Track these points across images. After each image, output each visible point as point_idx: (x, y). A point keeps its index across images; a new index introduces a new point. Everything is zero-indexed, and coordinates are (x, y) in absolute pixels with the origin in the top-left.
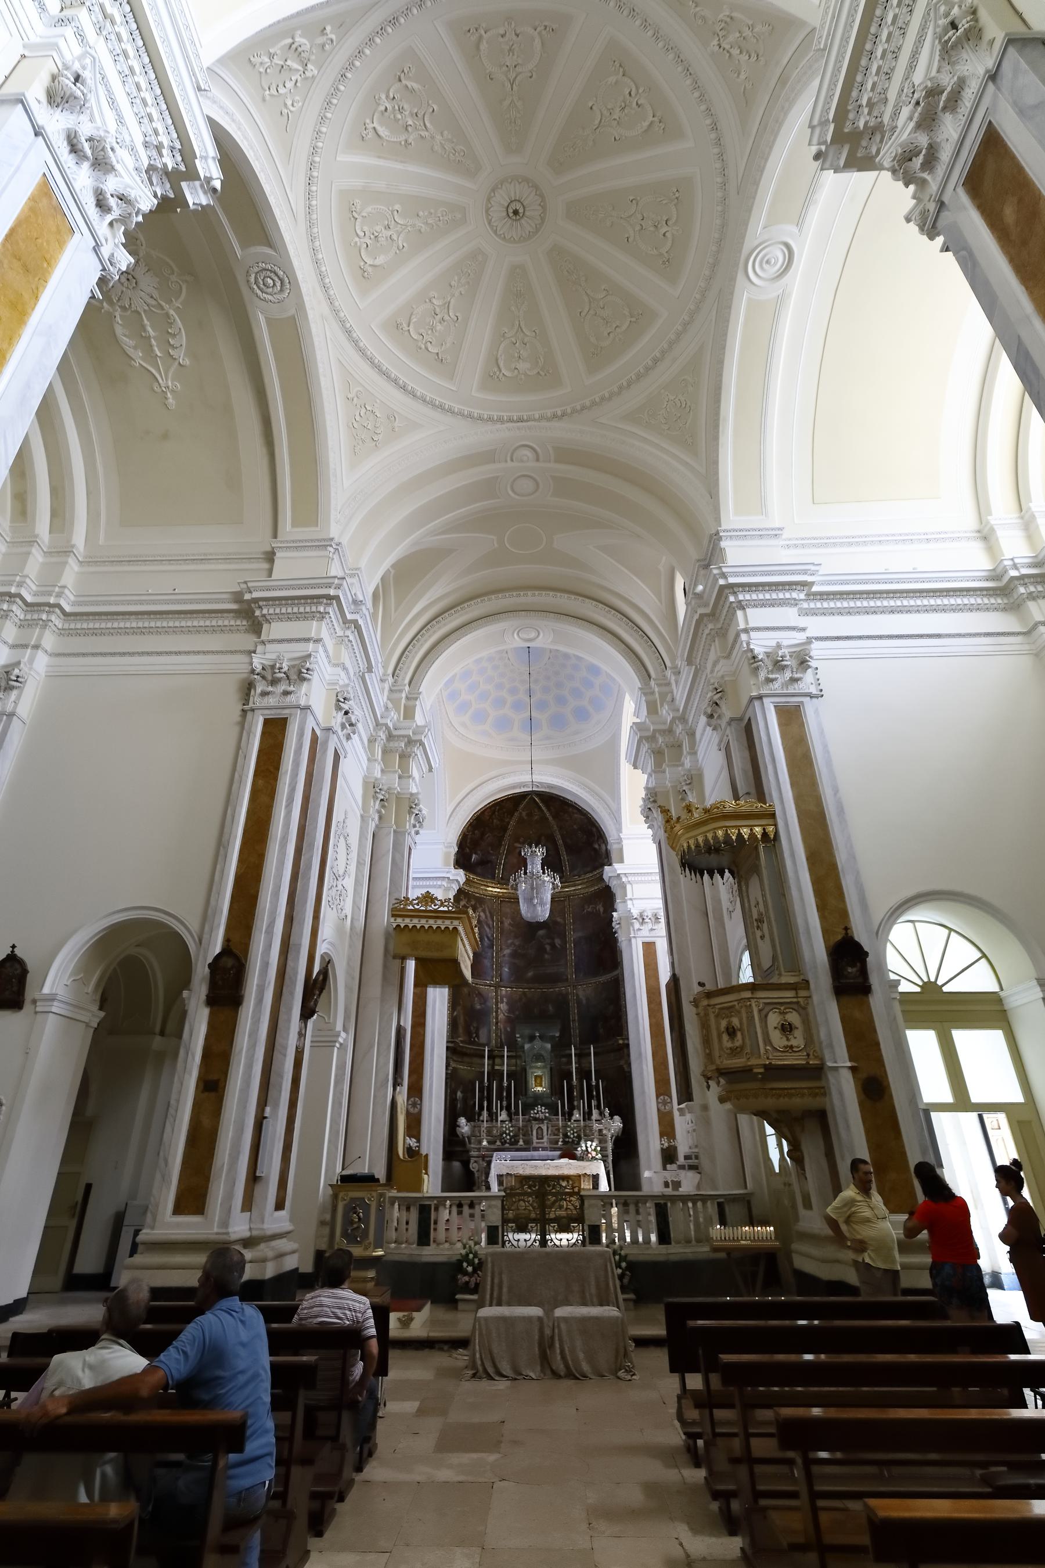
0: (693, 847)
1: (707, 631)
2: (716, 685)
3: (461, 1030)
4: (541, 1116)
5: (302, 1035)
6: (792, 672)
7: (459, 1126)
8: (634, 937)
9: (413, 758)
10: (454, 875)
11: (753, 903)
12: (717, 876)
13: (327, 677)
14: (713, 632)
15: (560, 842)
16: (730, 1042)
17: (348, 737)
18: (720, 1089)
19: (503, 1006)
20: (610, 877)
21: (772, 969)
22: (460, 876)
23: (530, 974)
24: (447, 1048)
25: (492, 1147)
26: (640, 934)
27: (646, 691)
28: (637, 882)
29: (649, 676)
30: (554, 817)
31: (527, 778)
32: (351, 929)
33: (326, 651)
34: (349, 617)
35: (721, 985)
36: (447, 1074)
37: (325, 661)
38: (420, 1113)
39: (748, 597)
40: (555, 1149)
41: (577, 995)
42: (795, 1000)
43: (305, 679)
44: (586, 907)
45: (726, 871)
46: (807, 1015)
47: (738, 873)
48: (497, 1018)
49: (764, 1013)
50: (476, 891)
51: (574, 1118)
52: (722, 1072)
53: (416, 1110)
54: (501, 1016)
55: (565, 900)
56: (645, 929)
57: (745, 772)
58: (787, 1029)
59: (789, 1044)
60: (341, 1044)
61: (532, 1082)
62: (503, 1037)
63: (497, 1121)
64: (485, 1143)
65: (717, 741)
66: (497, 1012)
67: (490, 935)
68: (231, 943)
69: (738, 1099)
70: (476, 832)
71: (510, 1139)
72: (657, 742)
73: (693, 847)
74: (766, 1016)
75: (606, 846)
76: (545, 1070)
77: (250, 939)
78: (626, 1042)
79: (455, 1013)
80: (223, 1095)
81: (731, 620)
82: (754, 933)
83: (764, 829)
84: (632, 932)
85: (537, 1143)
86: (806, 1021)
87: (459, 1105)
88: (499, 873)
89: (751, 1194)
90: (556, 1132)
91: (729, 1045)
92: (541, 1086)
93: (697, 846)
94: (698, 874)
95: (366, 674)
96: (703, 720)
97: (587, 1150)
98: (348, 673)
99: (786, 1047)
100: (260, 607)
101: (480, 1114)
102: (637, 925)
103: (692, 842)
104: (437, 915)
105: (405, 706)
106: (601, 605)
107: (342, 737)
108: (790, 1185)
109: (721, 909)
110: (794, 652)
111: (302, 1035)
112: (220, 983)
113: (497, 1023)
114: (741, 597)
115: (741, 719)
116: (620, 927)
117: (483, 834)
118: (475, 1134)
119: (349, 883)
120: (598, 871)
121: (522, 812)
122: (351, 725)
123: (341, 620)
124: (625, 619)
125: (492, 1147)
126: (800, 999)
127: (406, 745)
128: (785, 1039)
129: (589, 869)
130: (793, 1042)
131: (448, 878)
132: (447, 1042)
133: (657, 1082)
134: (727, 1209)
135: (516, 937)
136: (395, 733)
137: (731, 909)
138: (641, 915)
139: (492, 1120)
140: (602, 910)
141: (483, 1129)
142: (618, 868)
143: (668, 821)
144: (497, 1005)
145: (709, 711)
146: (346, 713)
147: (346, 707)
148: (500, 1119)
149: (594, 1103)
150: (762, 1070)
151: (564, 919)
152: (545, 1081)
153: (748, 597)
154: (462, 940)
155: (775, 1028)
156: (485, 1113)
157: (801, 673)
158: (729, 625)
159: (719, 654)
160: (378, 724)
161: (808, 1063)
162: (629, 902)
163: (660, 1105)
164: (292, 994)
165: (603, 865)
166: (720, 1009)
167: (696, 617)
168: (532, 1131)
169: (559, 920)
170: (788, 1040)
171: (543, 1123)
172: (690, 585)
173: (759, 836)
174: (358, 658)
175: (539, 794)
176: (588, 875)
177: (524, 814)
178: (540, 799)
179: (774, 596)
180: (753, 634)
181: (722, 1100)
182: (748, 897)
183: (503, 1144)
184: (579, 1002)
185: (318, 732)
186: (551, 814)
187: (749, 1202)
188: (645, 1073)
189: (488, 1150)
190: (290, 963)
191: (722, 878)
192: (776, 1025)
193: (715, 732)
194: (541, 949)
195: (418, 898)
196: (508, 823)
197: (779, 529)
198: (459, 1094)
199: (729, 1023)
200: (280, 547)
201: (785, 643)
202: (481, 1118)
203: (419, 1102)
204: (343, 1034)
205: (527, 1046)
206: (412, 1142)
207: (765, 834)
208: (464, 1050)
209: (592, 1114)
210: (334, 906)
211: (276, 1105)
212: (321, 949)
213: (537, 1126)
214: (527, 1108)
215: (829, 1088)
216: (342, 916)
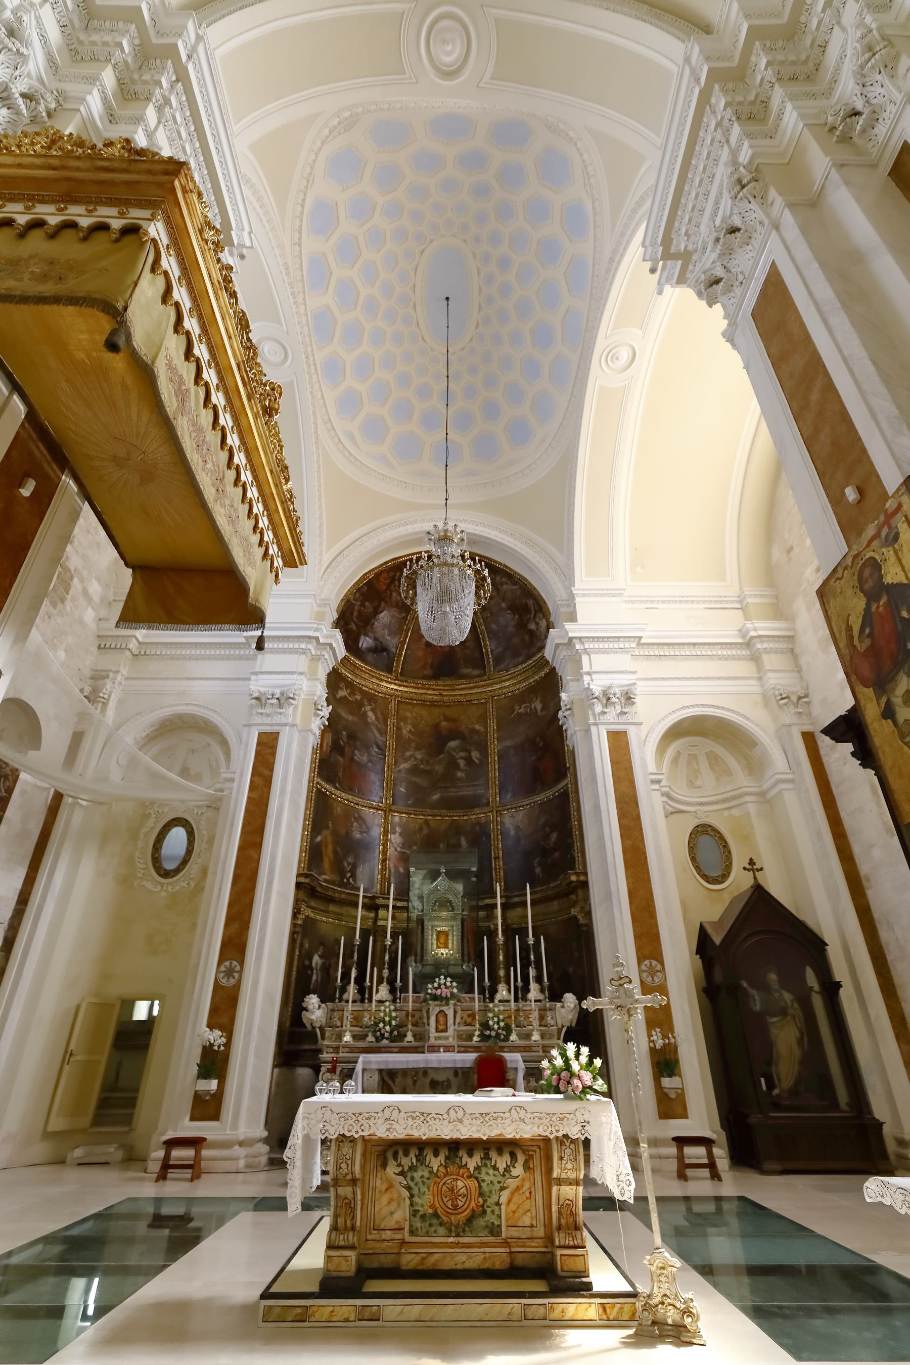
3: (326, 865)
4: (445, 992)
7: (306, 1009)
8: (596, 724)
10: (326, 637)
19: (395, 839)
23: (436, 797)
24: (298, 885)
25: (361, 1044)
26: (603, 719)
28: (598, 651)
36: (294, 925)
38: (237, 987)
39: (591, 646)
40: (465, 1050)
41: (502, 823)
44: (517, 707)
50: (363, 683)
51: (498, 997)
53: (232, 981)
54: (391, 852)
56: (612, 715)
61: (432, 941)
63: (370, 1001)
64: (347, 1038)
66: (385, 845)
67: (381, 743)
70: (367, 603)
71: (391, 1032)
76: (453, 923)
78: (582, 878)
79: (319, 839)
84: (591, 717)
85: (437, 1038)
87: (314, 977)
88: (398, 666)
90: (469, 1020)
92: (446, 947)
97: (568, 1066)
101: (344, 990)
102: (598, 708)
113: (384, 860)
114: (587, 646)
116: (572, 715)
118: (333, 1025)
125: (361, 1044)
129: (521, 659)
131: (317, 639)
132: (299, 875)
133: (637, 937)
135: (418, 748)
138: (605, 693)
139: (362, 1001)
140: (539, 706)
141: (346, 1014)
142: (572, 630)
148: (375, 997)
149: (532, 972)
151: (486, 727)
152: (454, 941)
153: (591, 646)
156: (352, 989)
162: (586, 678)
163: (645, 975)
168: (428, 1018)
169: (477, 727)
171: (447, 1004)
180: (594, 676)
183: (378, 1040)
188: (618, 923)
189: (352, 1050)
194: (453, 765)
198: (316, 960)
201: (617, 682)
202: (345, 997)
203: (238, 968)
206: (216, 1037)
208: (330, 893)
209: (528, 991)
213: (437, 1009)
214: (423, 979)
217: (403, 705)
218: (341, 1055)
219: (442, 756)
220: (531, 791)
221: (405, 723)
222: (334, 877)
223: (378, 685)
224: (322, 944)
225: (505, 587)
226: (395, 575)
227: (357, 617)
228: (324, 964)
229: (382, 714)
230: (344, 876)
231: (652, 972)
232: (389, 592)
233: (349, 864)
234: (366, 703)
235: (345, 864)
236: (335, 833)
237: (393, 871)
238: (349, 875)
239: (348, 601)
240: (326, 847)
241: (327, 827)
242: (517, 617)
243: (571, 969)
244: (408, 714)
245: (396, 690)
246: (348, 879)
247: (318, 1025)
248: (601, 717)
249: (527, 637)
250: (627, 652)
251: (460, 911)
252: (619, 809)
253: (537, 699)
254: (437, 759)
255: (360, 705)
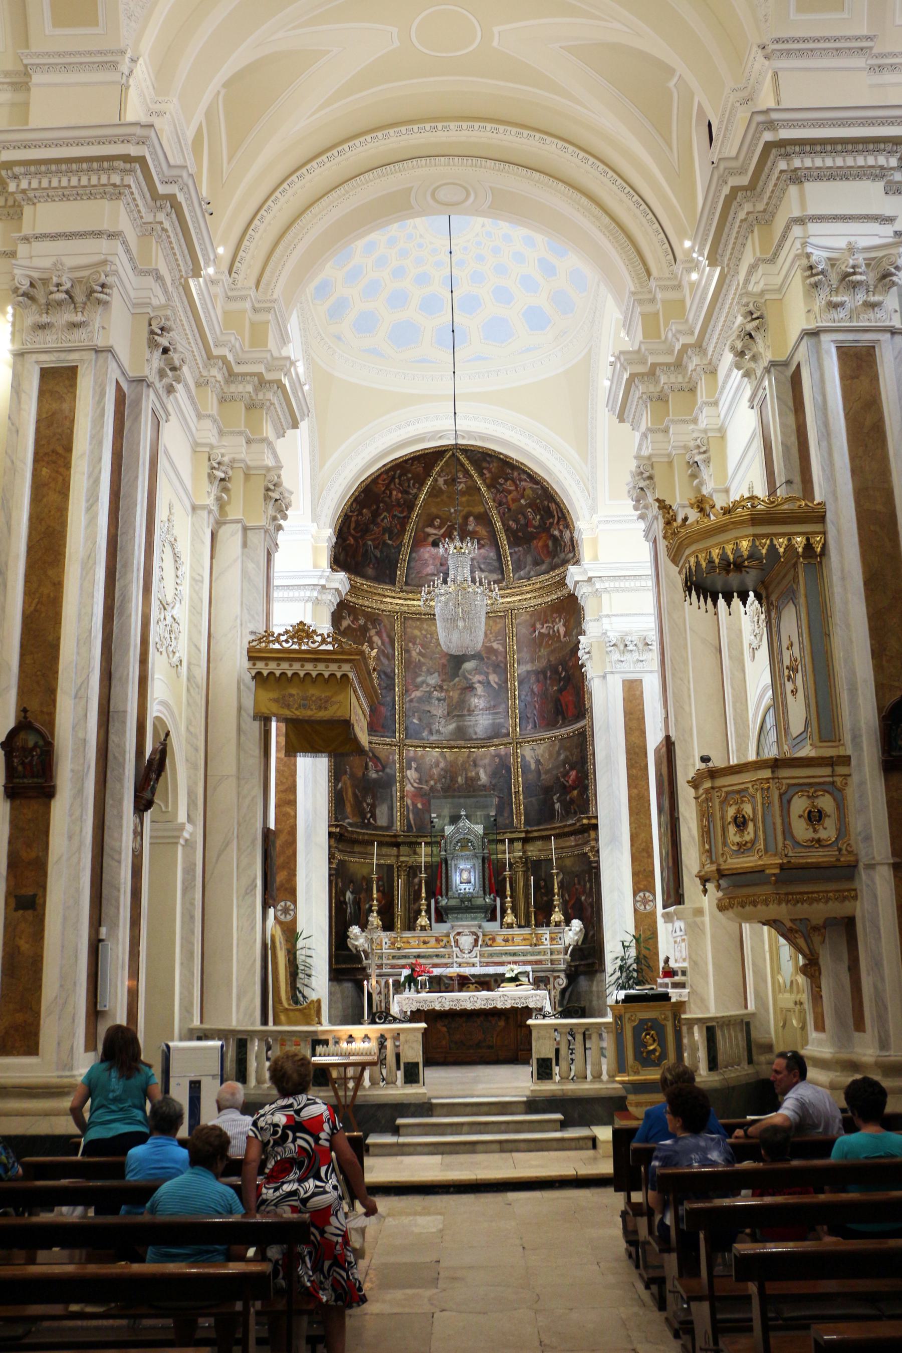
0: (704, 564)
1: (742, 215)
2: (751, 306)
3: (348, 809)
5: (138, 834)
6: (868, 292)
7: (348, 937)
9: (269, 408)
11: (785, 643)
12: (736, 601)
13: (132, 294)
14: (751, 218)
15: (499, 525)
16: (738, 835)
17: (170, 390)
18: (720, 894)
20: (577, 582)
21: (804, 735)
22: (340, 580)
24: (330, 834)
27: (642, 298)
29: (649, 273)
30: (489, 487)
31: (447, 424)
32: (188, 679)
33: (128, 251)
34: (162, 189)
35: (734, 761)
37: (128, 266)
41: (523, 756)
42: (830, 779)
43: (99, 302)
44: (538, 626)
45: (751, 594)
46: (844, 799)
47: (768, 597)
48: (402, 790)
49: (785, 798)
50: (367, 603)
52: (721, 874)
53: (289, 918)
55: (505, 616)
57: (786, 447)
58: (815, 817)
59: (816, 836)
60: (186, 840)
62: (411, 816)
65: (748, 393)
66: (401, 782)
68: (28, 714)
69: (743, 907)
70: (365, 511)
72: (657, 382)
73: (704, 564)
74: (789, 802)
75: (572, 533)
77: (55, 706)
78: (593, 821)
80: (44, 914)
81: (780, 199)
82: (783, 685)
83: (808, 539)
86: (841, 806)
87: (349, 910)
89: (753, 1015)
91: (737, 839)
93: (711, 561)
94: (709, 600)
95: (191, 281)
96: (728, 358)
98: (164, 285)
99: (813, 840)
100: (16, 177)
103: (702, 557)
104: (316, 657)
105: (252, 324)
106: (571, 148)
107: (161, 391)
108: (801, 1004)
109: (742, 643)
110: (874, 259)
111: (138, 834)
112: (20, 768)
113: (402, 798)
115: (786, 364)
116: (590, 658)
117: (375, 514)
119: (181, 611)
120: (557, 572)
121: (436, 478)
122: (174, 369)
123: (148, 195)
124: (611, 173)
126: (836, 779)
127: (256, 390)
128: (811, 830)
129: (544, 567)
130: (823, 834)
132: (330, 826)
133: (635, 874)
134: (719, 1034)
136: (237, 369)
137: (754, 646)
140: (562, 630)
143: (668, 523)
144: (402, 770)
145: (739, 345)
146: (165, 351)
147: (163, 341)
150: (777, 871)
154: (355, 691)
155: (800, 816)
157: (880, 294)
158: (777, 207)
159: (758, 254)
160: (210, 356)
161: (838, 860)
164: (120, 780)
165: (565, 562)
166: (727, 793)
167: (726, 190)
169: (495, 645)
170: (815, 831)
172: (721, 122)
173: (800, 550)
174: (178, 256)
175: (468, 451)
176: (543, 578)
177: (441, 481)
178: (468, 458)
179: (850, 161)
180: (813, 228)
181: (721, 908)
182: (779, 632)
184: (525, 767)
185: (125, 386)
186: (484, 481)
187: (748, 1024)
190: (113, 737)
191: (744, 604)
192: (801, 813)
193: (746, 379)
195: (287, 632)
196: (416, 497)
197: (869, 38)
198: (349, 895)
199: (739, 811)
200: (38, 65)
204: (189, 827)
205: (449, 830)
207: (808, 546)
208: (355, 836)
210: (163, 649)
211: (114, 926)
212: (154, 710)
215: (861, 891)
216: (175, 660)
217: (410, 622)
218: (384, 970)
219: (457, 679)
220: (551, 724)
221: (414, 644)
222: (357, 820)
223: (382, 602)
224: (352, 881)
225: (523, 483)
226: (395, 474)
227: (354, 529)
228: (355, 898)
229: (389, 636)
230: (365, 817)
231: (645, 902)
232: (388, 492)
233: (368, 805)
234: (370, 627)
235: (365, 805)
236: (353, 776)
237: (411, 807)
238: (369, 815)
239: (346, 515)
240: (346, 793)
241: (346, 773)
242: (538, 517)
243: (583, 898)
244: (417, 632)
245: (402, 605)
246: (369, 820)
247: (361, 949)
248: (618, 666)
249: (550, 543)
250: (876, 177)
251: (481, 851)
252: (629, 760)
253: (560, 621)
254: (452, 683)
255: (364, 630)
